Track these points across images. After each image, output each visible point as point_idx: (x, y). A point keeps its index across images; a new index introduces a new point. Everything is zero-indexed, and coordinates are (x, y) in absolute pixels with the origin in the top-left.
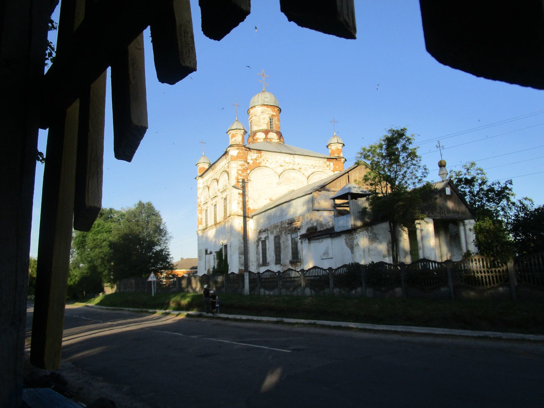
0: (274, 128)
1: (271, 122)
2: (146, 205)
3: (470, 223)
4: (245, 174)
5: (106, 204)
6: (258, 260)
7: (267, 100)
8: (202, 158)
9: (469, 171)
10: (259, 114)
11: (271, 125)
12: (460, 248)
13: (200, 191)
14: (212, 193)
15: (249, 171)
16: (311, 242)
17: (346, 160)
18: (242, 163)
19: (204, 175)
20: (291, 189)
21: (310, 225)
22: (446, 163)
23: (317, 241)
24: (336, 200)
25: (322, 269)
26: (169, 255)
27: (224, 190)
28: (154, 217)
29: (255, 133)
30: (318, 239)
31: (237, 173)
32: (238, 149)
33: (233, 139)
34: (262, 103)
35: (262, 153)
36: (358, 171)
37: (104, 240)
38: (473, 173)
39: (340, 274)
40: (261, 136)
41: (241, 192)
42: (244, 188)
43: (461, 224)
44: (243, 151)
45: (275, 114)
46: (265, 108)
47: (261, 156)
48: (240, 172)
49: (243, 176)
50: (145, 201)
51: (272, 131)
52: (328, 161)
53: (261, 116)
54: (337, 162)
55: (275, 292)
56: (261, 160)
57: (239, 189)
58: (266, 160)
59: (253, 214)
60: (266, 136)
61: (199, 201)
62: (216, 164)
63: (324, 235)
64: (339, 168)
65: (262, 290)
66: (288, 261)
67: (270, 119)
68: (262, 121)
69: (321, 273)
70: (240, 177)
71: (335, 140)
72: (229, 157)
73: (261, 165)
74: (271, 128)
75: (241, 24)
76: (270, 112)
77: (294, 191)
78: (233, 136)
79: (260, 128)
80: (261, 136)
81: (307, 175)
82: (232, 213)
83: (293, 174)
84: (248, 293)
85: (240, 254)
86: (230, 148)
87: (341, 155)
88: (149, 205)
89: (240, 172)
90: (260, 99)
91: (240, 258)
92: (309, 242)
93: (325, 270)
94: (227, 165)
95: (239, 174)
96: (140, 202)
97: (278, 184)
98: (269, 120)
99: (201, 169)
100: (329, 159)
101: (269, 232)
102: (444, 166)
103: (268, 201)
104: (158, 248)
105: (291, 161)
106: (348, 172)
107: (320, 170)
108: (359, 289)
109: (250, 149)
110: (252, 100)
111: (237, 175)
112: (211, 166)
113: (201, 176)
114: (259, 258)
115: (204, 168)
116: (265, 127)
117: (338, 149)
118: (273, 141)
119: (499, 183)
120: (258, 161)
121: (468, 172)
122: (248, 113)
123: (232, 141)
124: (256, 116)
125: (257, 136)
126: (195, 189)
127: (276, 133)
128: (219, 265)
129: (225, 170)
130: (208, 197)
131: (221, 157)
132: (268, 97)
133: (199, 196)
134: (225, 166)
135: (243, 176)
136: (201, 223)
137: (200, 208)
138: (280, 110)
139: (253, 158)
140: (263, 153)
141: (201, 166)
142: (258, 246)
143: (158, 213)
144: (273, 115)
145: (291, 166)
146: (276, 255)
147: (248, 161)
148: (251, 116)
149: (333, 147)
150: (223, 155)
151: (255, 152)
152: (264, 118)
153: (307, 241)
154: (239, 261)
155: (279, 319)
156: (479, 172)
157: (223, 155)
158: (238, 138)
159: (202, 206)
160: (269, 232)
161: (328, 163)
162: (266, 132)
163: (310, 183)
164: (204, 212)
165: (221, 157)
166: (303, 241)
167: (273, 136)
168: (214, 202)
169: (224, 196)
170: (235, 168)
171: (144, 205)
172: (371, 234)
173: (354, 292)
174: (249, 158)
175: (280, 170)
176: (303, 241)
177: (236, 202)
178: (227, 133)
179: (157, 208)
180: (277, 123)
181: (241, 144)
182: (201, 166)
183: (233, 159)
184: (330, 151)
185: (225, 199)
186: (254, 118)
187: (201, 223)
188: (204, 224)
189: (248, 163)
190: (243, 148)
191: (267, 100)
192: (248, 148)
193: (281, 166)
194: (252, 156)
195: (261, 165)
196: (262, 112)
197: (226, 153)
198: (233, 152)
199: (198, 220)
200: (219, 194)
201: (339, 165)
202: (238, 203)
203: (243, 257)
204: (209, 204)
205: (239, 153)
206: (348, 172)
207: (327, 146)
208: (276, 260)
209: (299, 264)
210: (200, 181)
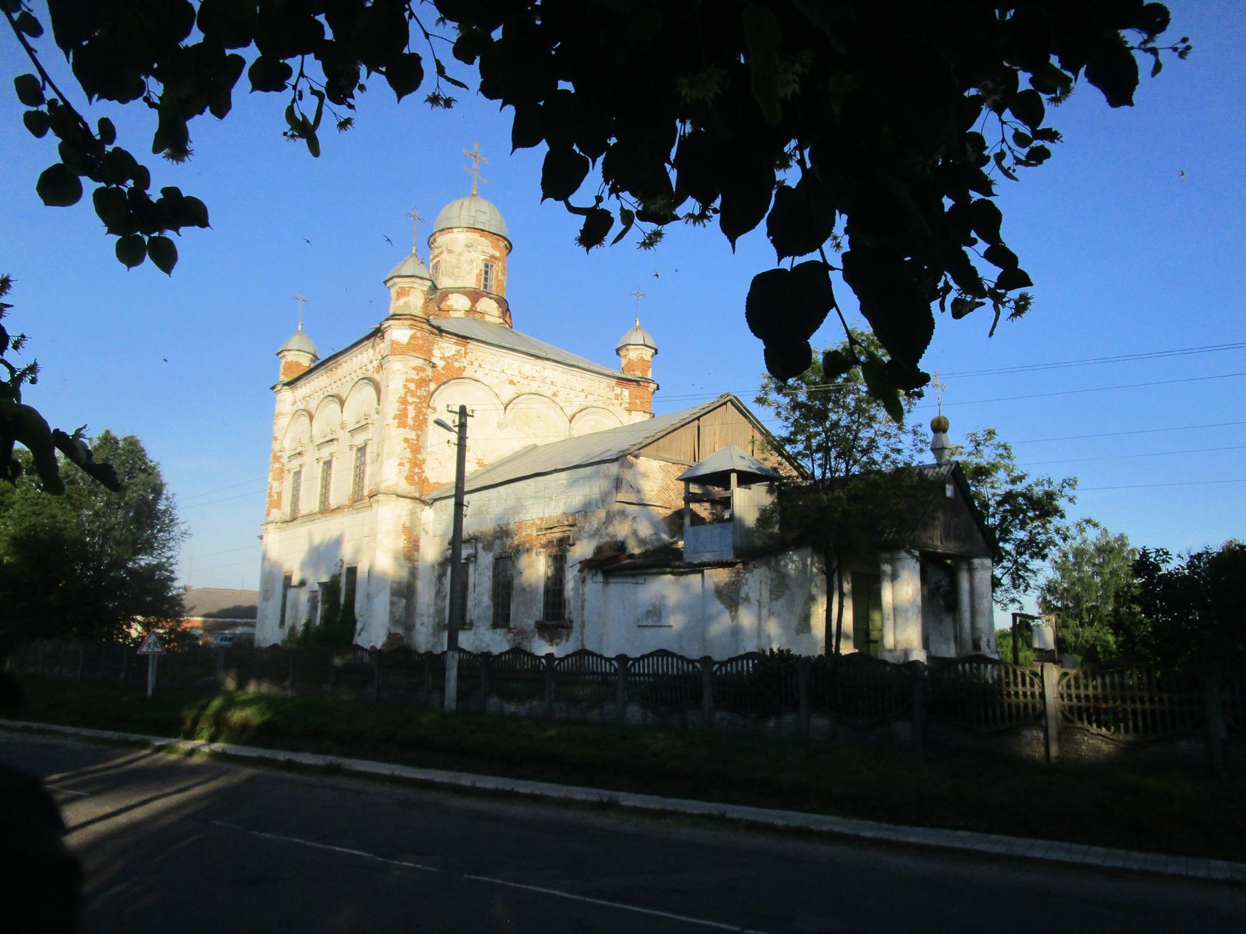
0: (494, 289)
1: (486, 273)
2: (121, 444)
3: (983, 565)
4: (422, 392)
6: (439, 611)
7: (482, 218)
8: (297, 338)
9: (981, 448)
10: (459, 248)
11: (486, 280)
12: (957, 619)
13: (282, 422)
14: (319, 429)
15: (432, 386)
16: (612, 580)
17: (658, 388)
18: (420, 362)
19: (300, 383)
20: (531, 441)
21: (607, 539)
22: (947, 424)
23: (630, 580)
24: (691, 486)
25: (683, 658)
26: (173, 580)
27: (363, 428)
28: (142, 476)
29: (445, 294)
30: (634, 576)
31: (405, 387)
33: (402, 301)
34: (471, 223)
35: (470, 346)
38: (987, 456)
39: (740, 674)
40: (459, 303)
41: (454, 437)
42: (462, 426)
43: (965, 566)
44: (423, 334)
45: (497, 254)
46: (476, 236)
47: (466, 353)
49: (419, 397)
50: (120, 434)
51: (488, 295)
52: (618, 384)
53: (463, 255)
54: (640, 389)
55: (535, 705)
56: (465, 362)
57: (449, 429)
58: (476, 364)
59: (435, 494)
61: (276, 446)
62: (342, 359)
63: (652, 567)
65: (494, 703)
66: (532, 623)
67: (487, 266)
68: (466, 266)
69: (672, 667)
70: (411, 399)
71: (637, 338)
72: (383, 346)
74: (485, 286)
75: (115, 102)
76: (486, 248)
77: (535, 447)
78: (403, 292)
79: (459, 284)
80: (459, 303)
81: (570, 412)
82: (382, 488)
83: (537, 405)
84: (454, 706)
86: (391, 322)
87: (649, 376)
88: (131, 444)
89: (412, 386)
90: (465, 212)
91: (392, 604)
92: (606, 583)
93: (691, 662)
94: (376, 363)
95: (408, 390)
96: (108, 432)
97: (500, 425)
98: (482, 267)
99: (289, 366)
100: (623, 381)
101: (480, 546)
102: (945, 431)
104: (144, 560)
105: (537, 375)
106: (698, 418)
107: (599, 403)
108: (789, 719)
109: (441, 331)
110: (443, 212)
111: (403, 391)
112: (320, 365)
113: (289, 384)
114: (443, 609)
115: (298, 364)
116: (471, 282)
117: (642, 358)
118: (488, 318)
119: (1050, 483)
120: (456, 365)
121: (978, 451)
122: (431, 242)
123: (396, 306)
124: (450, 252)
125: (449, 303)
126: (270, 415)
127: (497, 301)
128: (327, 617)
129: (369, 374)
130: (305, 440)
131: (362, 341)
132: (483, 212)
133: (277, 434)
134: (370, 367)
135: (419, 397)
136: (277, 504)
137: (278, 465)
138: (510, 247)
140: (472, 345)
141: (290, 357)
142: (441, 577)
143: (153, 469)
144: (493, 257)
145: (534, 387)
146: (496, 605)
147: (433, 360)
148: (437, 251)
149: (633, 354)
150: (368, 338)
151: (454, 339)
152: (472, 261)
153: (600, 578)
154: (392, 613)
156: (1001, 451)
157: (368, 338)
158: (415, 301)
159: (285, 460)
160: (480, 546)
161: (618, 390)
162: (475, 296)
163: (575, 434)
164: (289, 479)
165: (362, 341)
166: (588, 578)
167: (489, 306)
168: (325, 453)
169: (359, 440)
170: (399, 374)
171: (117, 442)
172: (774, 575)
173: (772, 724)
175: (508, 392)
176: (588, 578)
177: (394, 461)
178: (385, 282)
179: (153, 453)
180: (500, 277)
181: (421, 315)
182: (290, 357)
183: (397, 349)
184: (624, 362)
185: (362, 450)
186: (445, 256)
187: (277, 504)
188: (286, 508)
189: (434, 366)
190: (426, 326)
191: (482, 218)
192: (438, 328)
193: (512, 382)
194: (445, 349)
195: (464, 375)
196: (467, 246)
197: (378, 333)
198: (399, 333)
199: (270, 496)
200: (344, 436)
202: (401, 464)
204: (308, 458)
205: (413, 337)
206: (698, 418)
207: (618, 351)
208: (496, 615)
209: (564, 631)
210: (286, 396)
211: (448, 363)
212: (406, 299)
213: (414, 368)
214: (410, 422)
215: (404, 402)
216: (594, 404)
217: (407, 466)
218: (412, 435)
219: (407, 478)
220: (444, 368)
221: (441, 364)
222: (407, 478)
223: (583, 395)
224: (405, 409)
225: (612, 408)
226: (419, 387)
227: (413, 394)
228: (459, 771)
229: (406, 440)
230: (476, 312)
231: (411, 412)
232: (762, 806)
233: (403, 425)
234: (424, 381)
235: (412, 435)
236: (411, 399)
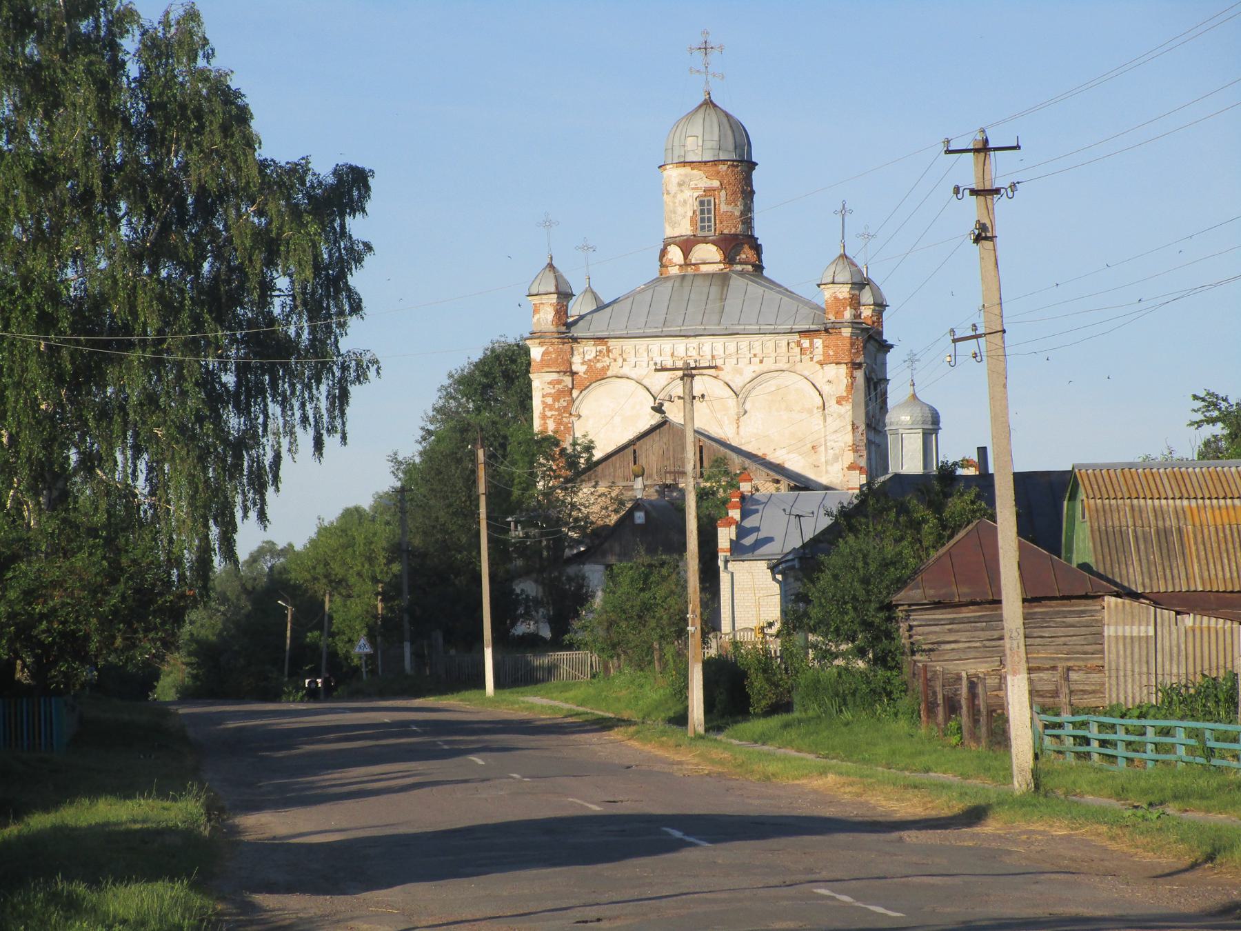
1: (702, 212)
5: (690, 233)
36: (657, 438)
45: (716, 183)
46: (687, 170)
47: (609, 351)
48: (549, 400)
49: (558, 409)
51: (705, 240)
60: (686, 257)
64: (836, 353)
67: (702, 203)
68: (680, 210)
70: (549, 414)
73: (609, 373)
89: (549, 400)
98: (696, 206)
116: (685, 229)
117: (836, 298)
120: (599, 365)
127: (714, 243)
139: (587, 357)
147: (575, 368)
152: (685, 202)
155: (797, 782)
161: (806, 343)
162: (687, 245)
195: (609, 373)
205: (544, 354)
211: (590, 367)
213: (550, 383)
226: (556, 399)
227: (551, 408)
228: (487, 825)
232: (348, 840)
236: (549, 414)
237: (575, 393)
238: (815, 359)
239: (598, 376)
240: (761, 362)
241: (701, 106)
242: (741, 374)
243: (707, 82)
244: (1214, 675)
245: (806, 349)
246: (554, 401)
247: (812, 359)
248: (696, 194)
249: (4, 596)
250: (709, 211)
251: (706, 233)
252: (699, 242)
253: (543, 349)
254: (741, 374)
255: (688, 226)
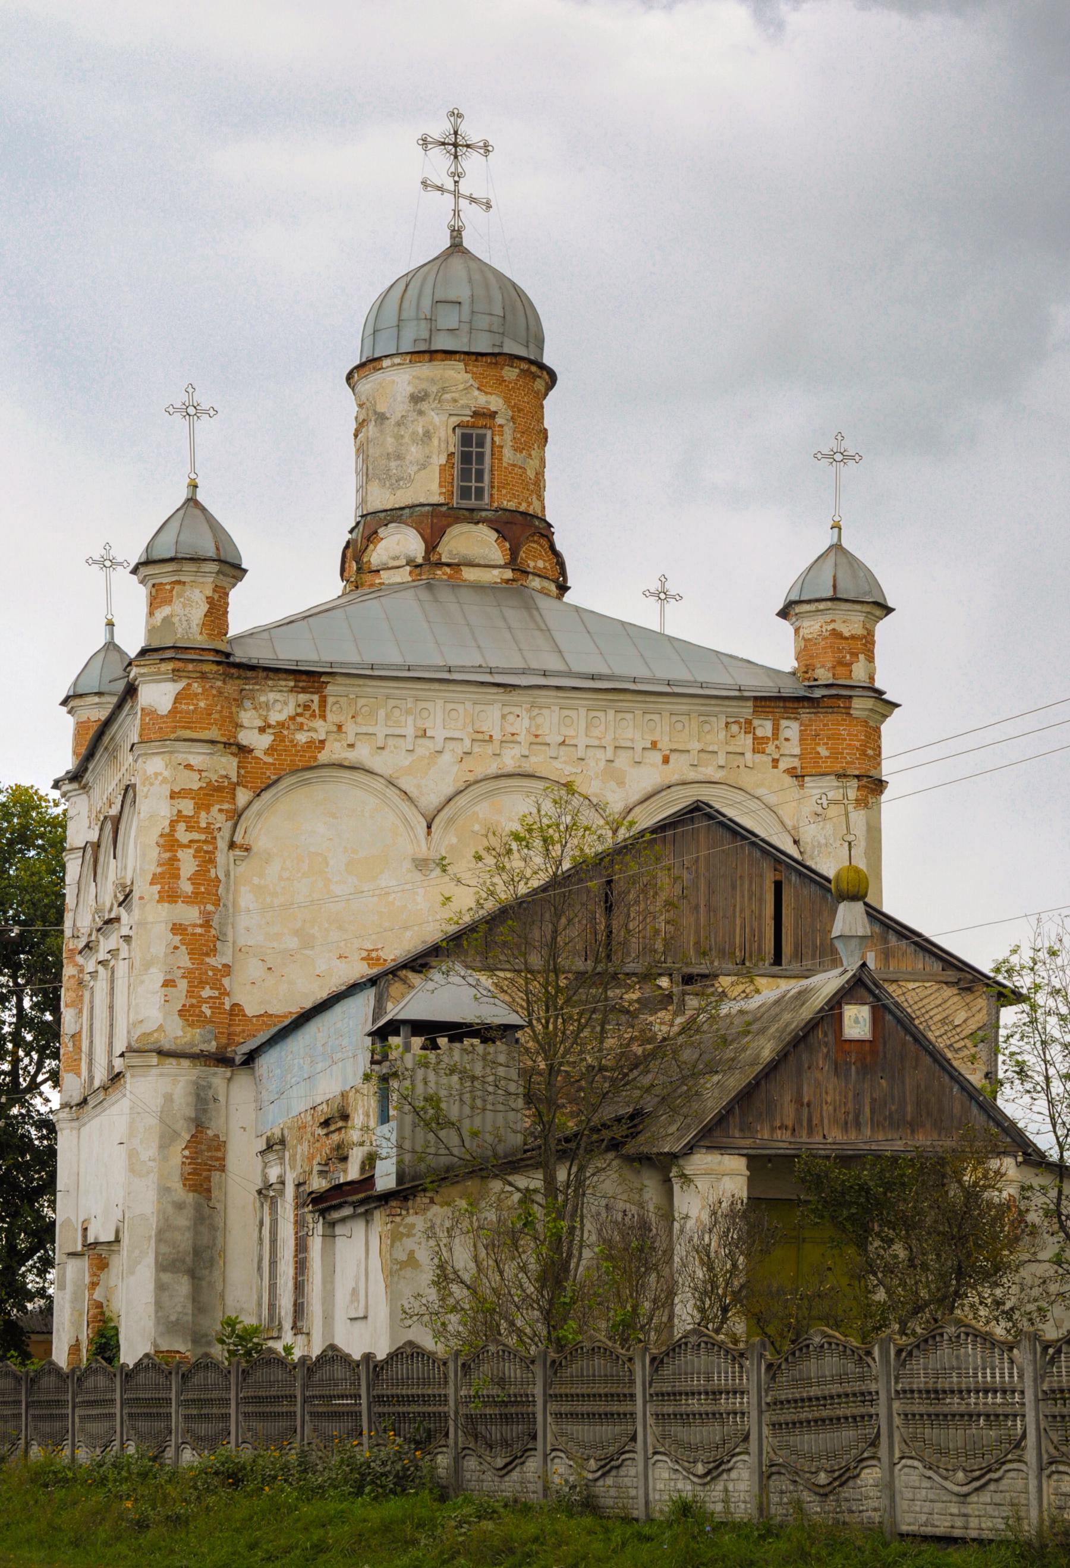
1: (466, 458)
16: (339, 1230)
32: (176, 675)
35: (330, 689)
37: (709, 732)
51: (471, 516)
54: (826, 722)
60: (431, 547)
64: (835, 755)
67: (466, 440)
68: (414, 452)
73: (323, 757)
85: (163, 1266)
89: (187, 807)
91: (160, 1287)
98: (453, 444)
103: (358, 976)
120: (302, 738)
139: (275, 717)
140: (267, 1062)
147: (246, 737)
152: (427, 435)
154: (159, 1305)
161: (764, 728)
174: (248, 717)
177: (156, 977)
181: (200, 640)
195: (323, 757)
196: (416, 399)
201: (834, 737)
202: (168, 983)
203: (183, 1286)
205: (178, 698)
211: (279, 737)
212: (166, 611)
214: (187, 887)
215: (170, 843)
216: (692, 775)
217: (183, 985)
218: (190, 914)
219: (181, 1013)
220: (270, 750)
221: (260, 743)
222: (181, 1013)
223: (657, 757)
224: (174, 859)
225: (747, 779)
229: (177, 929)
230: (440, 564)
231: (188, 864)
233: (170, 896)
234: (219, 789)
235: (190, 914)
236: (183, 835)
237: (243, 796)
238: (783, 765)
239: (302, 764)
240: (666, 760)
241: (184, 504)
242: (621, 783)
243: (456, 213)
244: (501, 1374)
245: (764, 740)
246: (198, 807)
247: (775, 762)
248: (454, 420)
249: (1068, 1130)
250: (480, 476)
251: (472, 503)
252: (457, 520)
253: (180, 686)
254: (621, 783)
255: (435, 486)
